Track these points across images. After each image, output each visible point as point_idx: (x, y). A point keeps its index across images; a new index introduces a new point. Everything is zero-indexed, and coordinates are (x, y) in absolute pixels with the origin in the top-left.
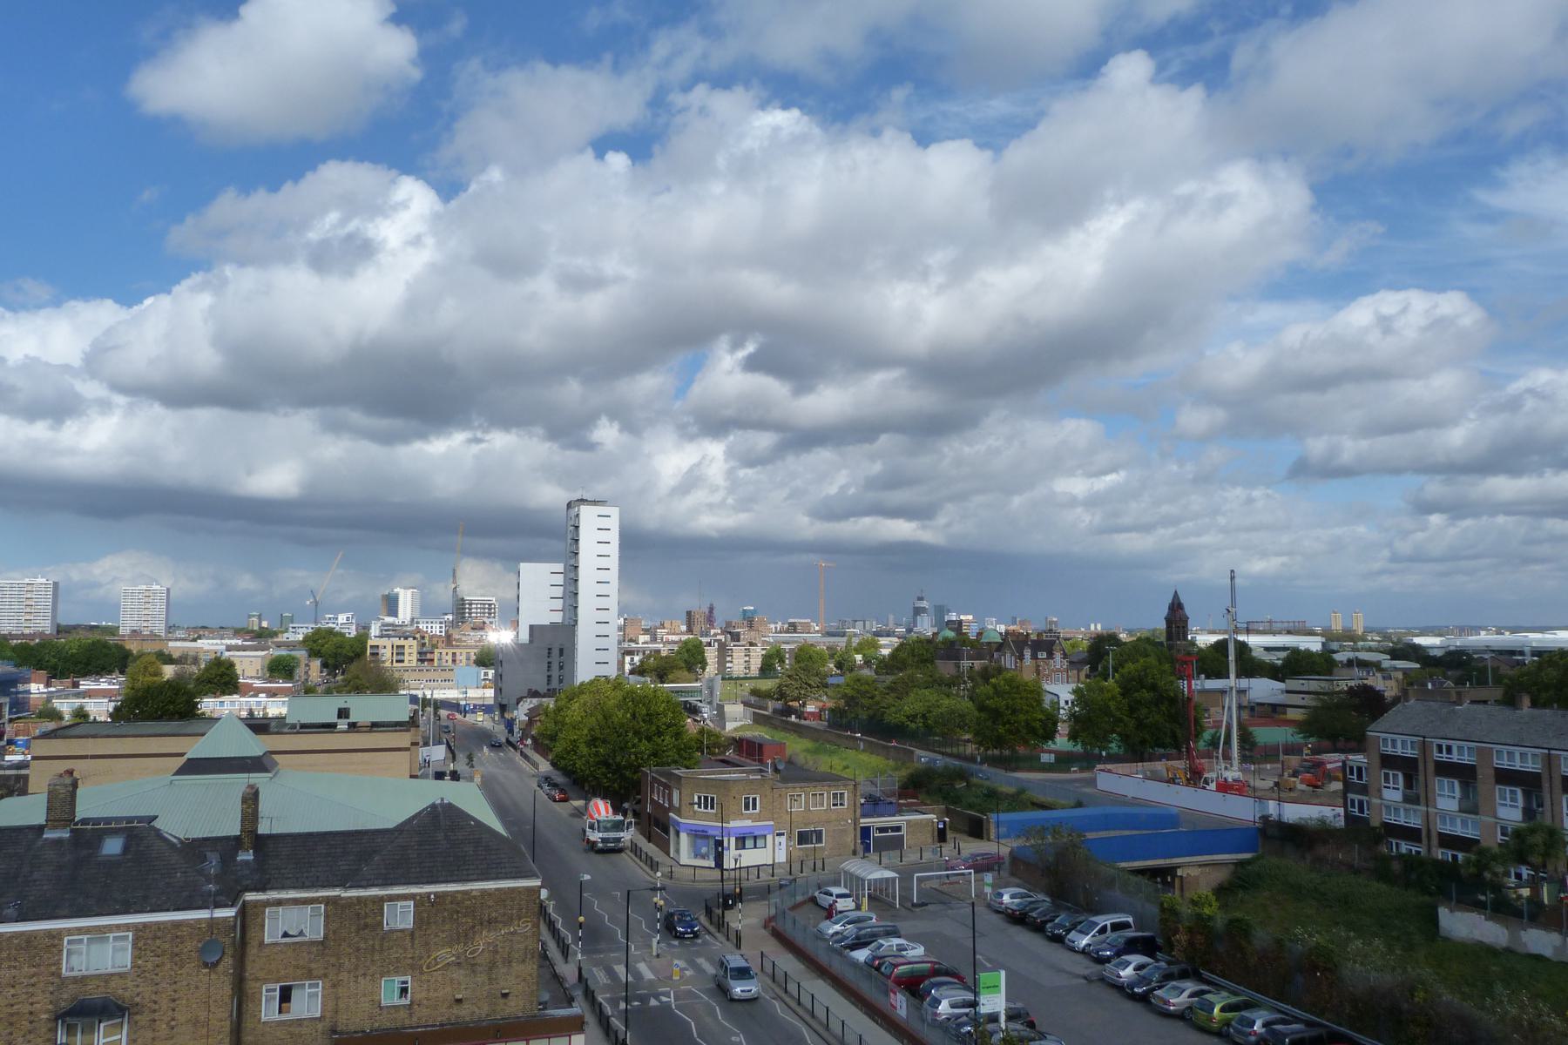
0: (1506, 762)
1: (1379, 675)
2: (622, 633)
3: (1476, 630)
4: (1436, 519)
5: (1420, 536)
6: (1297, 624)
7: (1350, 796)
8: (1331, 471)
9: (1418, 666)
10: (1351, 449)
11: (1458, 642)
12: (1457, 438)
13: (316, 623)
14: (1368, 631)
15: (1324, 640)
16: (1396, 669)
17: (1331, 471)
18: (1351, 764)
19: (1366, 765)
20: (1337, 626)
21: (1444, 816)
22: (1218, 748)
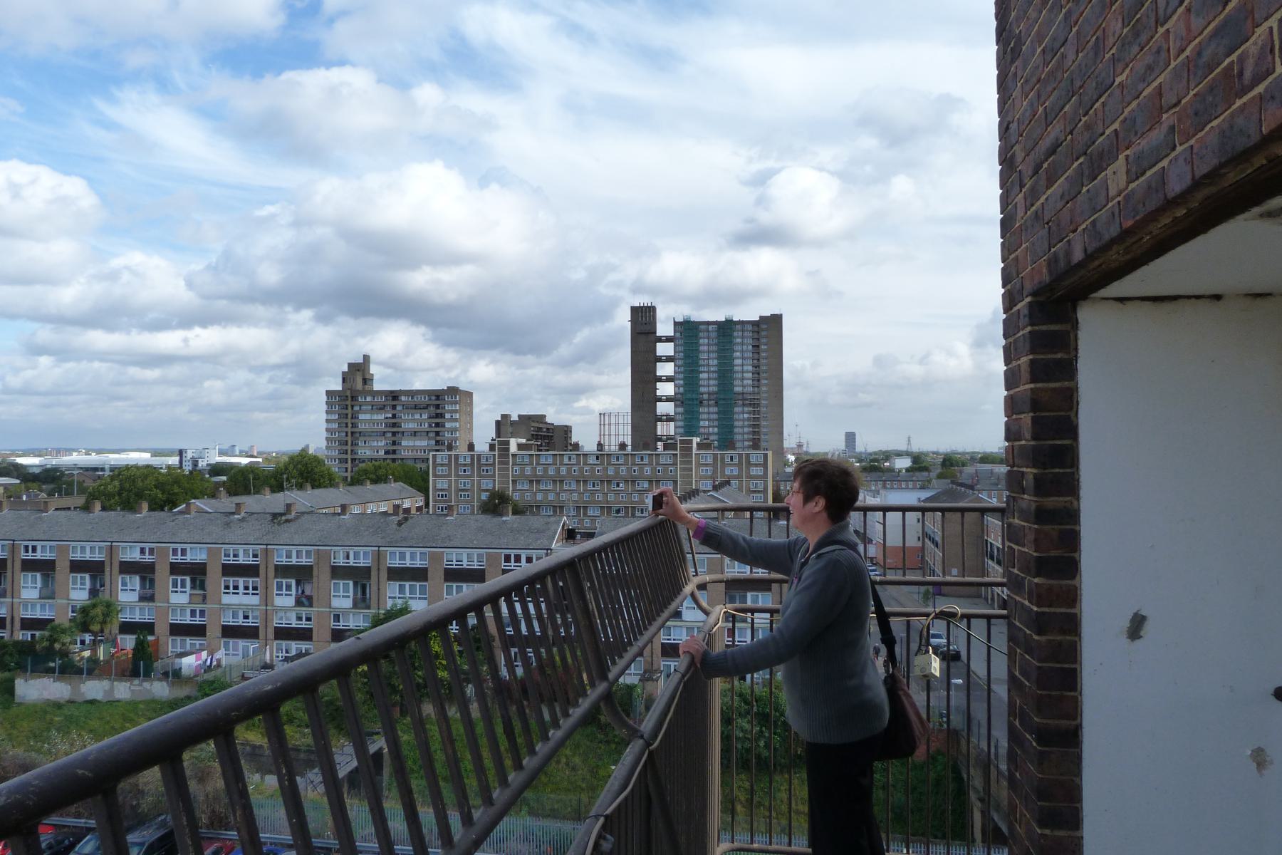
2: (237, 453)
3: (69, 451)
4: (44, 361)
5: (29, 374)
9: (18, 481)
11: (54, 461)
12: (68, 296)
21: (25, 604)
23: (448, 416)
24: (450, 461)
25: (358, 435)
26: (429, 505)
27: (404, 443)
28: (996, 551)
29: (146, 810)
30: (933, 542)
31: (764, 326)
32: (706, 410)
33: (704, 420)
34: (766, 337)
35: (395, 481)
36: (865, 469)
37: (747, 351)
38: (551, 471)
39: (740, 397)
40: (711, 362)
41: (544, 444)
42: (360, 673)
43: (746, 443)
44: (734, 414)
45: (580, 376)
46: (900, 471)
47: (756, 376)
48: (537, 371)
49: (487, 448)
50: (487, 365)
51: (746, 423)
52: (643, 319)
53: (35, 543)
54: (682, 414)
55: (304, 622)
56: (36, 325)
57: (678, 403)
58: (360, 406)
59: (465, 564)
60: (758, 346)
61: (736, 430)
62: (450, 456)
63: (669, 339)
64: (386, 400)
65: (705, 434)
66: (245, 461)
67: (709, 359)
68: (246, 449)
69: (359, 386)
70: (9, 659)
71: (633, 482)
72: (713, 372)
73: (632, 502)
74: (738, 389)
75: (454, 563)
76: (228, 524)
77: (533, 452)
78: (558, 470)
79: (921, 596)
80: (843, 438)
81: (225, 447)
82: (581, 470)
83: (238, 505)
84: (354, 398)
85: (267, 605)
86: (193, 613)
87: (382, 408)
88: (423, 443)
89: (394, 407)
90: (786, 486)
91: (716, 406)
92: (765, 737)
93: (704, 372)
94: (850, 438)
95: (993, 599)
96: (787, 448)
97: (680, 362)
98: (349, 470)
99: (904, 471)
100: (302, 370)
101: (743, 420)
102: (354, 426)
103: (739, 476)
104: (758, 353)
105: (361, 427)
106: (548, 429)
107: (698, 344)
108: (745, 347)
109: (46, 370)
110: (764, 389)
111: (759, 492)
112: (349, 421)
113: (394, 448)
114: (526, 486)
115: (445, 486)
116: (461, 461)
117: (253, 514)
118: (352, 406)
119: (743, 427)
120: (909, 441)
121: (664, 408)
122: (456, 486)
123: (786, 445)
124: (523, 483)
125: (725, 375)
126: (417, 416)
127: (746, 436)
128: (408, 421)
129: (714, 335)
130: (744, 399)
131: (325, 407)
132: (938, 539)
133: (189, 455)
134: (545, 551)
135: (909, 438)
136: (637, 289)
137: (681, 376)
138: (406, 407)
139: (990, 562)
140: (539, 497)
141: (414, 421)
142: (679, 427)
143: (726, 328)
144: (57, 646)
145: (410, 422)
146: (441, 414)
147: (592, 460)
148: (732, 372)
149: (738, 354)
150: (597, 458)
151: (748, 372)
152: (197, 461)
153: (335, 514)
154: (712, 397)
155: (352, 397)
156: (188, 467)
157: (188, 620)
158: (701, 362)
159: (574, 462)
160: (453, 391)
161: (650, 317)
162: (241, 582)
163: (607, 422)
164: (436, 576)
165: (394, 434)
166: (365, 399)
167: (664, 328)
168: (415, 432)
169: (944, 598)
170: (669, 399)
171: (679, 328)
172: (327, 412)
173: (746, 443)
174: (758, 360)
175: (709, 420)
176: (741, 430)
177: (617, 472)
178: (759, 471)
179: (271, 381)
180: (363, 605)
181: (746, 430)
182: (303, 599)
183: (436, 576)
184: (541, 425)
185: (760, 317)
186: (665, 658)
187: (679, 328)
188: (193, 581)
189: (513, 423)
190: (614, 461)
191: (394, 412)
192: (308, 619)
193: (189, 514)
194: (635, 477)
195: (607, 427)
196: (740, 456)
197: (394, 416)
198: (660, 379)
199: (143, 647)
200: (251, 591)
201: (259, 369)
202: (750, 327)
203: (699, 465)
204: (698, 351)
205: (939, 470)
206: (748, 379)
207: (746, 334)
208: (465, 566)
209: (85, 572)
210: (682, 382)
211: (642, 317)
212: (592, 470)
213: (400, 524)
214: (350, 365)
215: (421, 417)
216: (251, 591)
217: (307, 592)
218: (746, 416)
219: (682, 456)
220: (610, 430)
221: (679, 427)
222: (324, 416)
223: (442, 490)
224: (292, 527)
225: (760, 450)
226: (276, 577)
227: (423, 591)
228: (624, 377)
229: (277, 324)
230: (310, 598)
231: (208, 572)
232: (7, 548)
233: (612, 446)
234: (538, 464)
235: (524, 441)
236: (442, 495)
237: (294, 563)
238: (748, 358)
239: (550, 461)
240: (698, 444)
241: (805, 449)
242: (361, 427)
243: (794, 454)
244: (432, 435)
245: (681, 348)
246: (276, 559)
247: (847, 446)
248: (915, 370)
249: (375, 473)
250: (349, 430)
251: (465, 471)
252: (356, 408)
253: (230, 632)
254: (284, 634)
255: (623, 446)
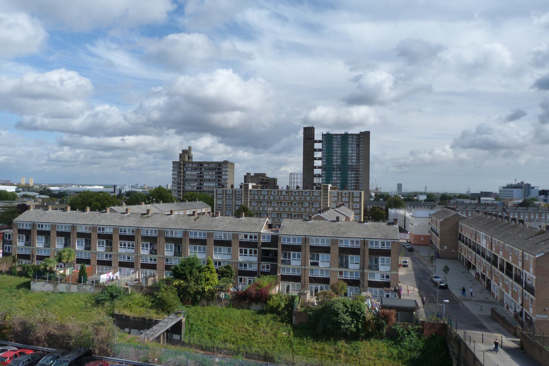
0: (60, 229)
1: (33, 200)
2: (139, 187)
3: (72, 185)
4: (66, 148)
5: (60, 153)
6: (7, 181)
7: (5, 245)
8: (32, 128)
9: (49, 197)
10: (40, 121)
11: (64, 189)
12: (77, 123)
13: (145, 287)
14: (35, 184)
15: (16, 187)
16: (40, 198)
17: (32, 128)
18: (5, 233)
19: (12, 234)
20: (23, 182)
21: (38, 249)
22: (499, 264)
23: (223, 173)
24: (223, 192)
25: (185, 180)
26: (214, 211)
27: (205, 184)
28: (465, 238)
29: (72, 345)
30: (436, 234)
31: (362, 136)
32: (335, 173)
33: (335, 177)
34: (362, 141)
35: (199, 201)
36: (405, 200)
37: (354, 147)
38: (266, 198)
39: (351, 167)
40: (338, 152)
41: (265, 186)
42: (174, 286)
43: (353, 187)
44: (348, 174)
45: (283, 157)
46: (422, 201)
47: (358, 158)
48: (264, 156)
49: (239, 187)
50: (243, 152)
51: (353, 179)
52: (309, 132)
53: (42, 224)
54: (325, 174)
55: (153, 261)
56: (62, 134)
57: (323, 169)
58: (187, 168)
59: (223, 238)
60: (359, 145)
61: (349, 182)
62: (223, 190)
63: (320, 142)
64: (198, 166)
65: (334, 183)
66: (141, 190)
67: (337, 150)
68: (143, 186)
69: (187, 160)
70: (29, 272)
71: (302, 203)
72: (339, 156)
73: (260, 211)
74: (350, 164)
75: (218, 238)
76: (122, 218)
77: (259, 189)
78: (259, 197)
79: (430, 258)
80: (396, 186)
81: (134, 184)
82: (279, 198)
83: (127, 210)
84: (184, 165)
85: (137, 253)
86: (107, 256)
87: (196, 169)
88: (213, 184)
89: (201, 169)
90: (370, 207)
91: (340, 171)
92: (354, 323)
93: (335, 156)
94: (400, 186)
95: (463, 261)
96: (371, 190)
97: (324, 152)
98: (182, 195)
99: (423, 201)
100: (166, 153)
101: (352, 177)
102: (184, 176)
103: (349, 202)
104: (359, 148)
105: (187, 177)
106: (267, 180)
107: (332, 144)
108: (353, 146)
109: (66, 152)
110: (361, 164)
111: (357, 209)
112: (182, 174)
113: (201, 186)
114: (255, 204)
115: (221, 203)
116: (228, 193)
117: (133, 213)
118: (183, 168)
119: (351, 180)
120: (426, 188)
121: (317, 171)
122: (226, 203)
123: (371, 188)
124: (254, 203)
125: (344, 157)
126: (211, 173)
127: (353, 184)
128: (207, 175)
129: (340, 140)
130: (352, 168)
131: (172, 168)
132: (438, 232)
133: (118, 187)
134: (258, 234)
135: (426, 186)
136: (305, 120)
137: (325, 158)
138: (206, 169)
139: (462, 244)
140: (261, 209)
141: (209, 175)
142: (323, 180)
143: (345, 137)
144: (48, 268)
145: (207, 175)
146: (221, 172)
147: (284, 193)
148: (347, 156)
149: (350, 148)
150: (286, 193)
151: (354, 156)
152: (121, 190)
153: (168, 215)
154: (338, 167)
155: (183, 164)
156: (117, 194)
157: (104, 259)
158: (334, 152)
159: (276, 194)
160: (226, 162)
161: (312, 131)
162: (127, 242)
163: (293, 177)
164: (210, 243)
165: (201, 180)
166: (189, 165)
167: (318, 136)
168: (210, 180)
169: (440, 259)
170: (319, 168)
171: (324, 137)
172: (173, 171)
173: (353, 187)
174: (359, 151)
175: (337, 177)
176: (350, 182)
177: (295, 199)
178: (358, 200)
179: (154, 157)
180: (178, 255)
181: (353, 182)
182: (153, 252)
183: (210, 243)
184: (264, 178)
185: (360, 132)
186: (310, 283)
187: (324, 137)
188: (107, 242)
189: (252, 177)
190: (294, 194)
191: (201, 171)
192: (155, 260)
193: (127, 214)
194: (303, 201)
195: (293, 179)
196: (349, 193)
197: (201, 173)
198: (315, 159)
199: (83, 271)
200: (131, 247)
201: (149, 153)
202: (355, 137)
203: (331, 196)
204: (333, 147)
205: (439, 201)
206: (354, 159)
207: (353, 140)
208: (223, 239)
209: (63, 236)
210: (325, 160)
211: (308, 132)
212: (284, 198)
213: (195, 220)
214: (183, 151)
215: (212, 173)
216: (131, 247)
217: (155, 248)
218: (353, 175)
219: (324, 192)
220: (294, 180)
221: (323, 180)
222: (172, 172)
223: (219, 205)
224: (150, 219)
225: (346, 190)
226: (142, 241)
227: (204, 249)
228: (300, 159)
229: (159, 134)
230: (156, 251)
231: (113, 238)
232: (31, 225)
233: (293, 187)
234: (261, 194)
235: (255, 184)
236: (220, 207)
237: (149, 235)
238: (354, 150)
239: (266, 193)
240: (331, 187)
241: (379, 190)
242: (187, 177)
243: (374, 193)
244: (217, 181)
245: (325, 146)
246: (142, 234)
247: (398, 190)
248: (427, 156)
249: (190, 197)
250: (182, 178)
251: (229, 197)
252: (185, 169)
253: (122, 264)
254: (144, 266)
255: (298, 187)
